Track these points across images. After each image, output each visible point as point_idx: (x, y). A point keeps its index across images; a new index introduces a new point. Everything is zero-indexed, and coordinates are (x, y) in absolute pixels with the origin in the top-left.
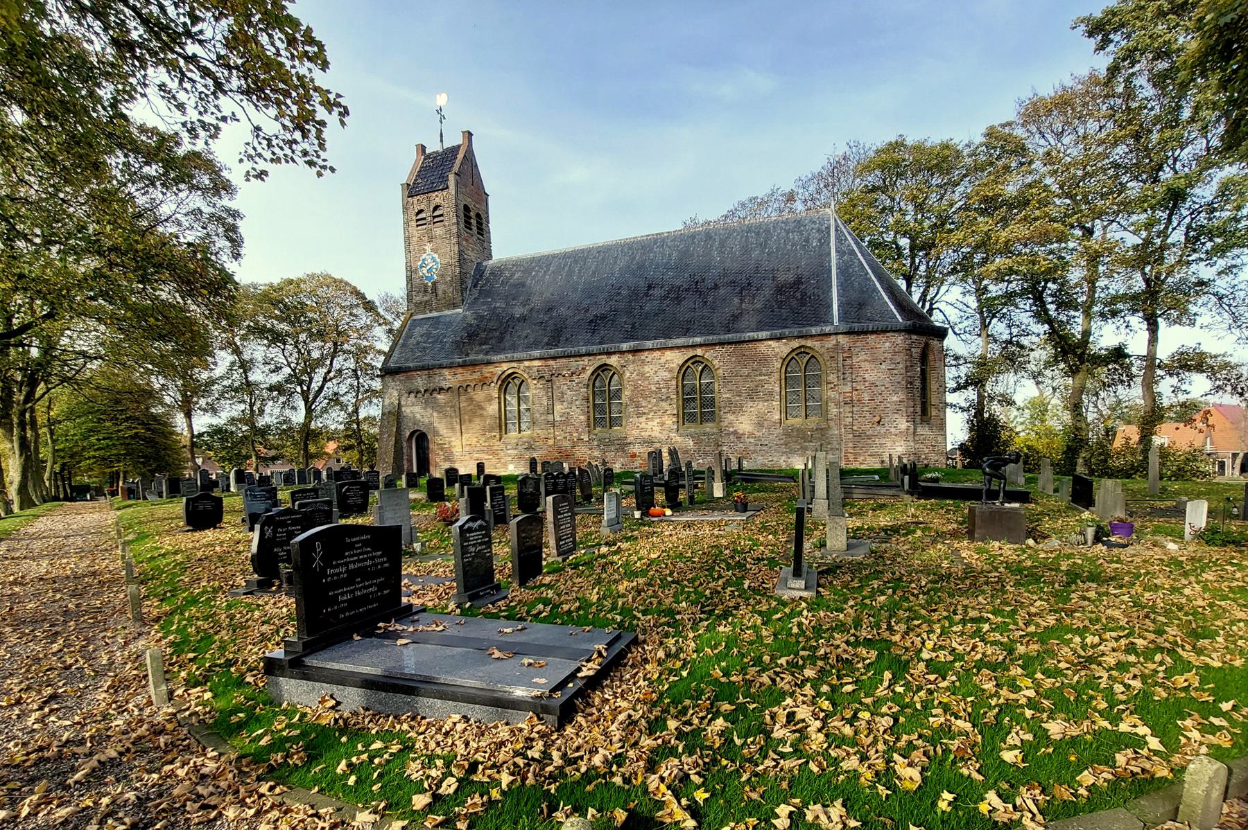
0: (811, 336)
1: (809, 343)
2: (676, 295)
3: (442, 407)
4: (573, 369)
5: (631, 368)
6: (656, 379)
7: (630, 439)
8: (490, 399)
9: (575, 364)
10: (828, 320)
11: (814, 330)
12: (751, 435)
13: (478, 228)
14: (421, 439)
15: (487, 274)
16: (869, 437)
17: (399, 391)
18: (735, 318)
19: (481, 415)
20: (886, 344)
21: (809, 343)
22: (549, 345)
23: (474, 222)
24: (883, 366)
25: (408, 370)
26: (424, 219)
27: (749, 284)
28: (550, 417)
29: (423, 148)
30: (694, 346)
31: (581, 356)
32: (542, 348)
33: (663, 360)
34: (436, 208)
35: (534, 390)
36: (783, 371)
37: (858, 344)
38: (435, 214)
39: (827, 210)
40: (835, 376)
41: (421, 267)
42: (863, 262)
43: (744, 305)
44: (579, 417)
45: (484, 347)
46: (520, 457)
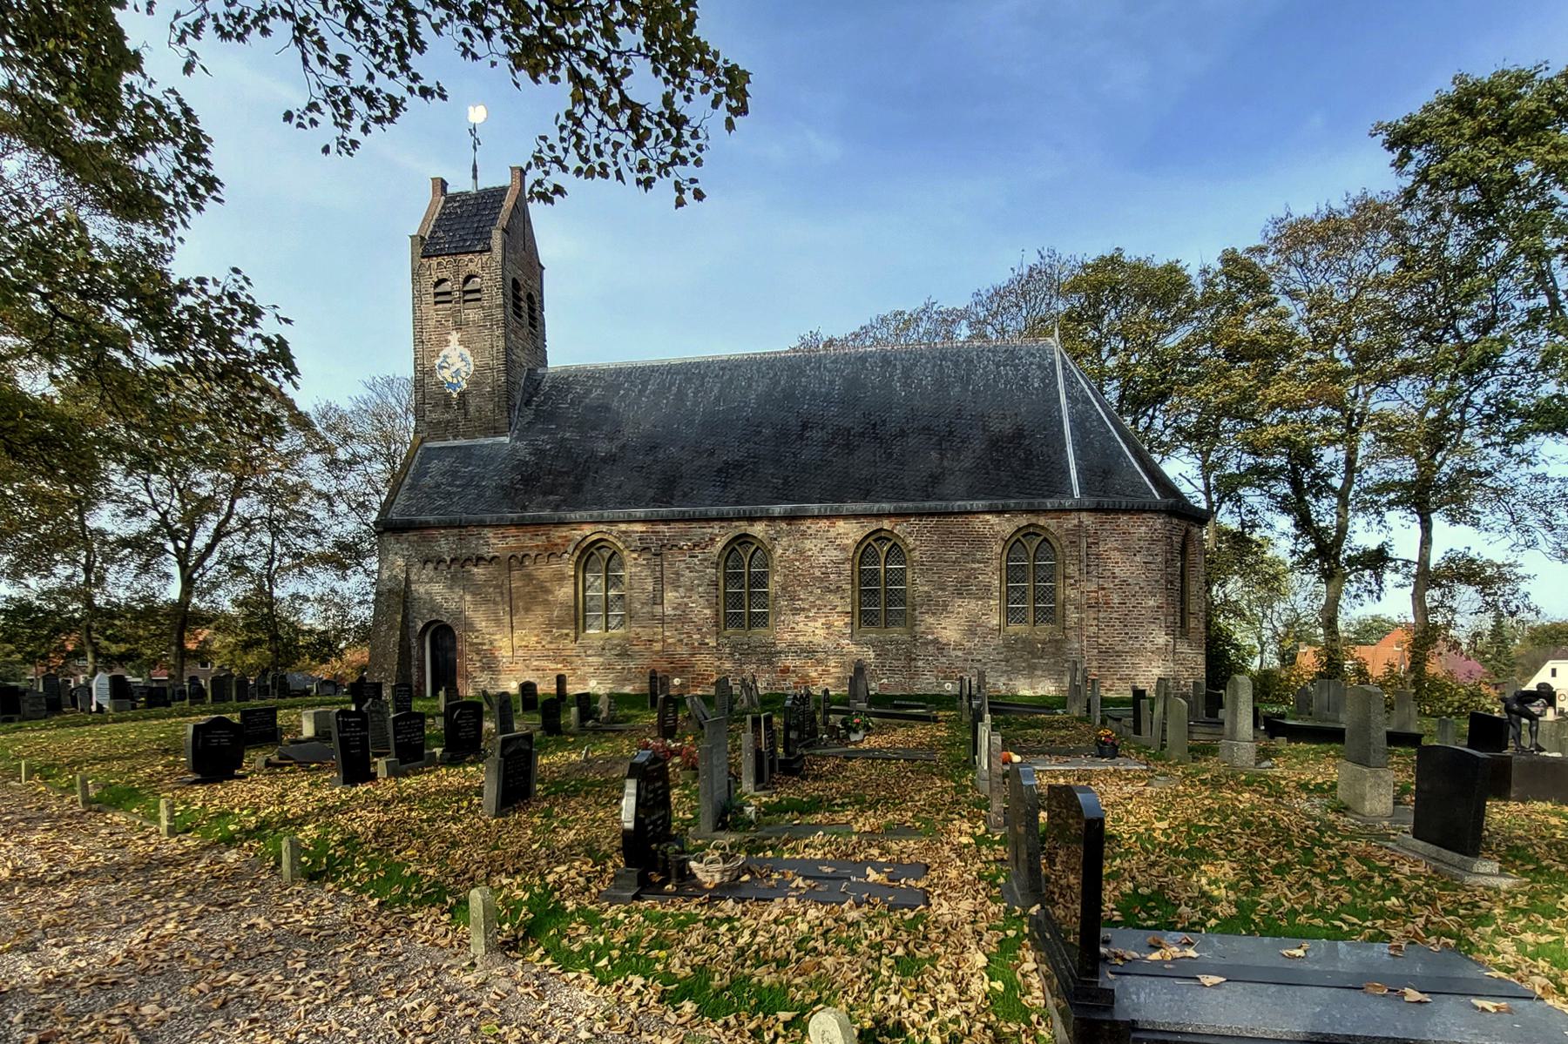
0: (1045, 511)
1: (1042, 521)
2: (846, 441)
3: (479, 587)
4: (697, 539)
5: (784, 541)
6: (822, 560)
7: (781, 646)
8: (560, 578)
9: (699, 531)
10: (1063, 488)
11: (1049, 503)
12: (957, 647)
13: (530, 316)
14: (443, 635)
15: (546, 386)
16: (1118, 654)
17: (408, 558)
18: (935, 479)
19: (546, 603)
20: (1142, 528)
21: (1042, 521)
22: (656, 501)
23: (524, 305)
24: (1138, 558)
25: (427, 526)
26: (449, 293)
27: (951, 433)
28: (658, 609)
29: (444, 184)
30: (879, 516)
31: (709, 520)
32: (647, 506)
33: (832, 533)
34: (467, 280)
35: (634, 568)
36: (1004, 558)
37: (1107, 526)
38: (468, 287)
39: (1049, 340)
40: (1076, 568)
41: (441, 368)
42: (1103, 414)
43: (945, 463)
44: (702, 611)
45: (551, 498)
46: (608, 667)
